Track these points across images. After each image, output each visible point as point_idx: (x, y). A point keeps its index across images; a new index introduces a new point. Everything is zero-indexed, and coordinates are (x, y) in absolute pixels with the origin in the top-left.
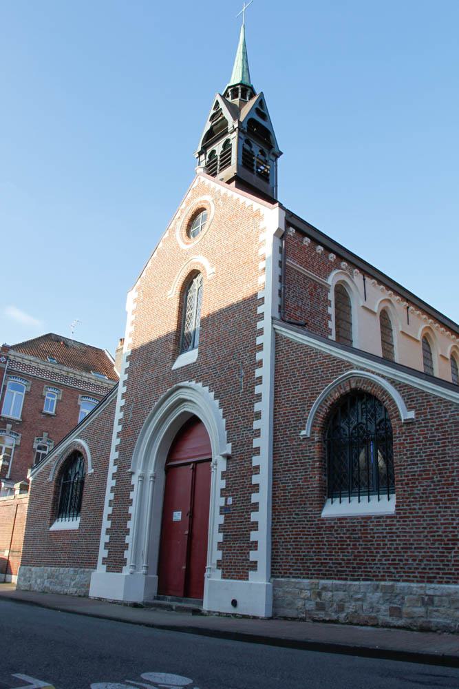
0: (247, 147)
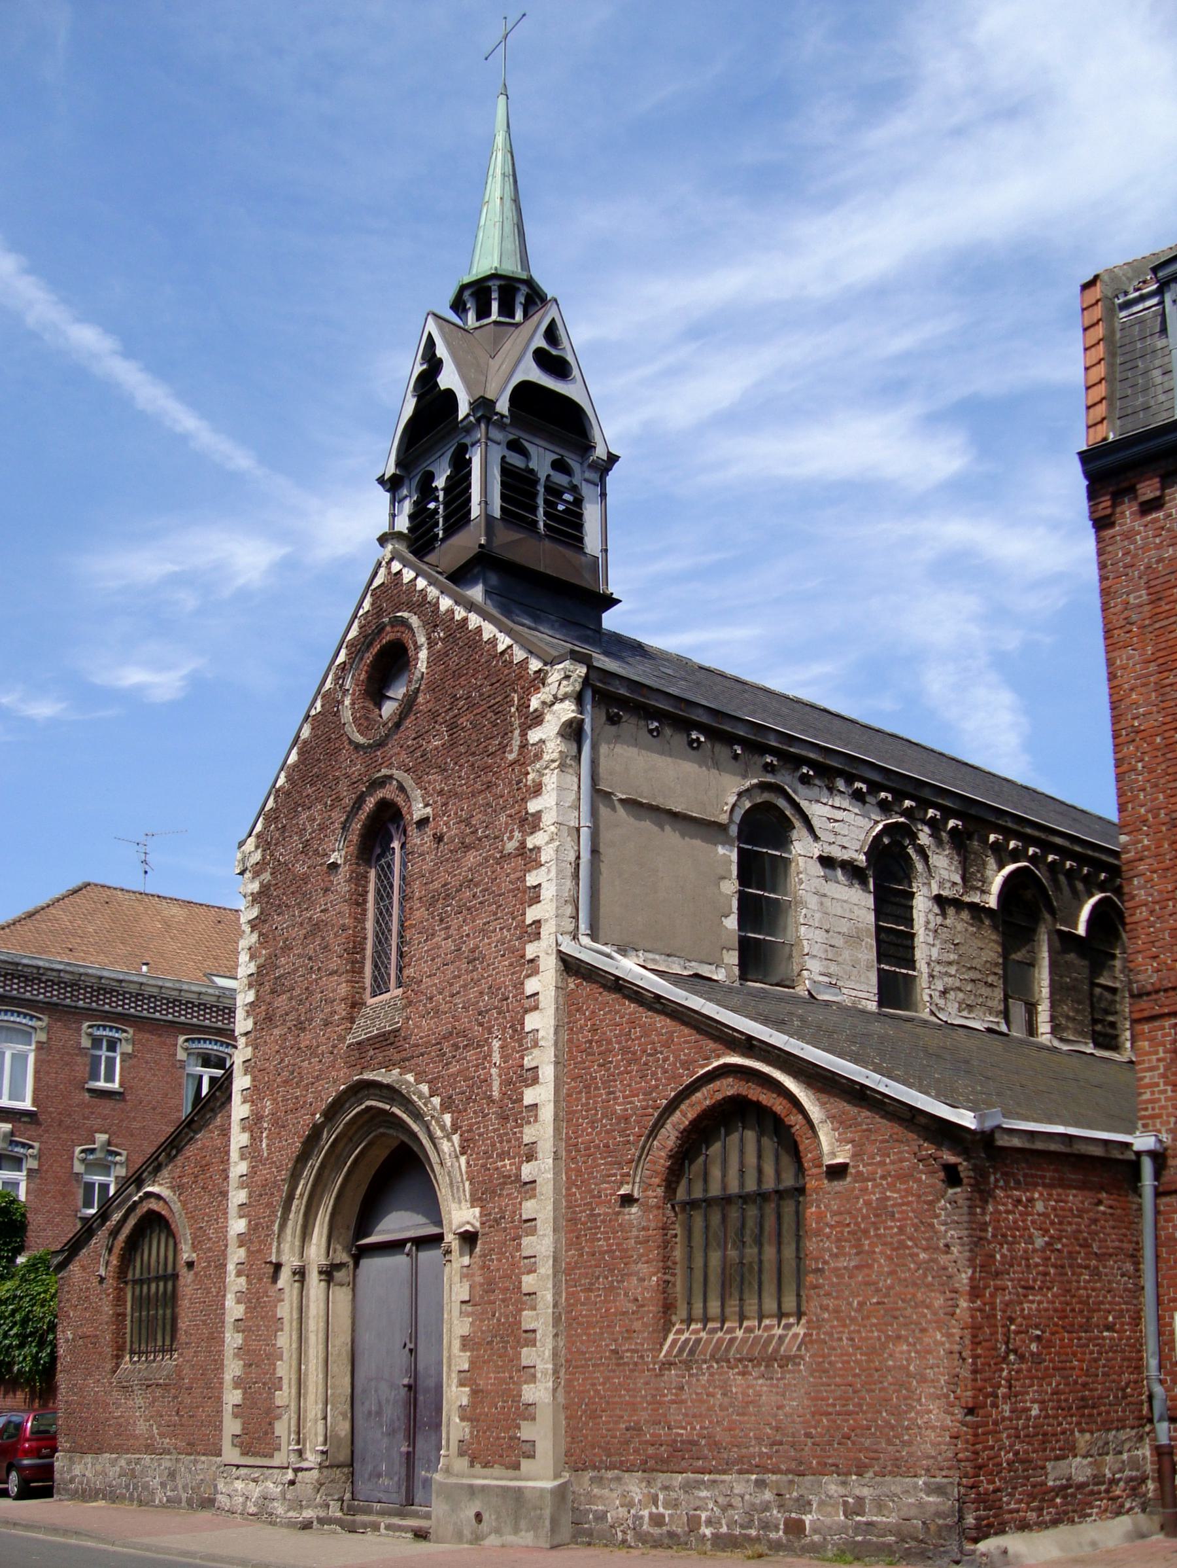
0: (516, 460)
